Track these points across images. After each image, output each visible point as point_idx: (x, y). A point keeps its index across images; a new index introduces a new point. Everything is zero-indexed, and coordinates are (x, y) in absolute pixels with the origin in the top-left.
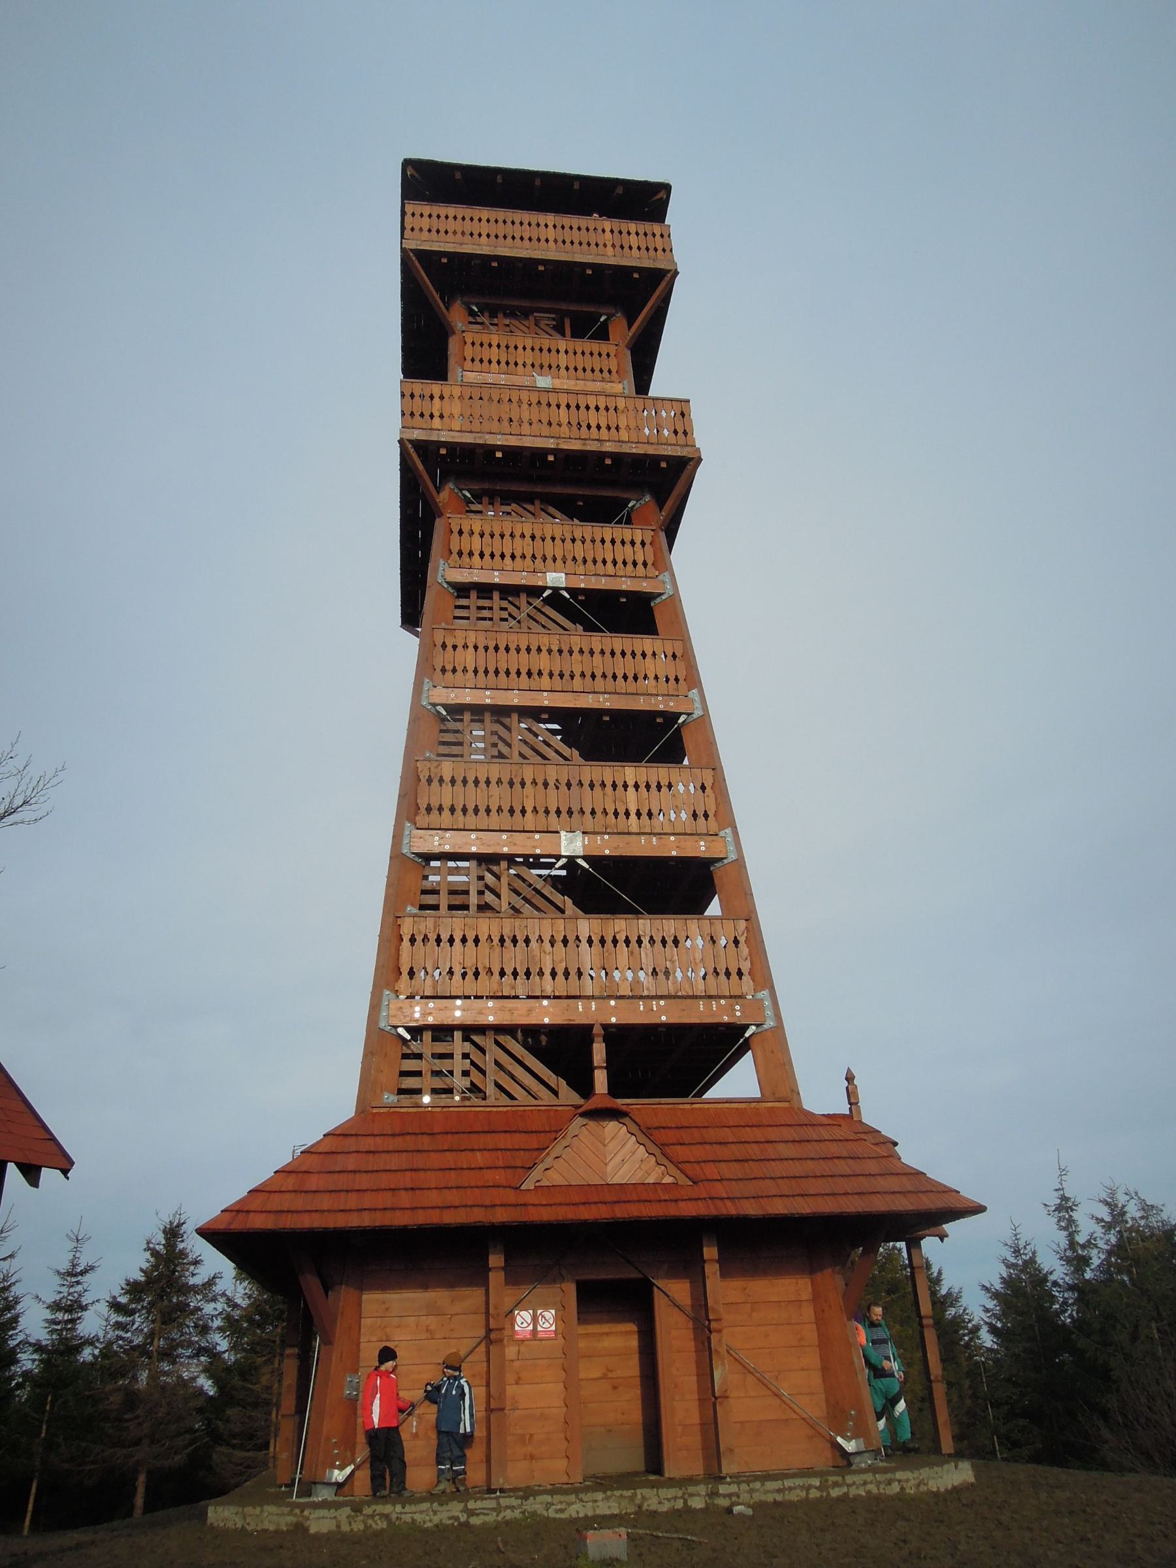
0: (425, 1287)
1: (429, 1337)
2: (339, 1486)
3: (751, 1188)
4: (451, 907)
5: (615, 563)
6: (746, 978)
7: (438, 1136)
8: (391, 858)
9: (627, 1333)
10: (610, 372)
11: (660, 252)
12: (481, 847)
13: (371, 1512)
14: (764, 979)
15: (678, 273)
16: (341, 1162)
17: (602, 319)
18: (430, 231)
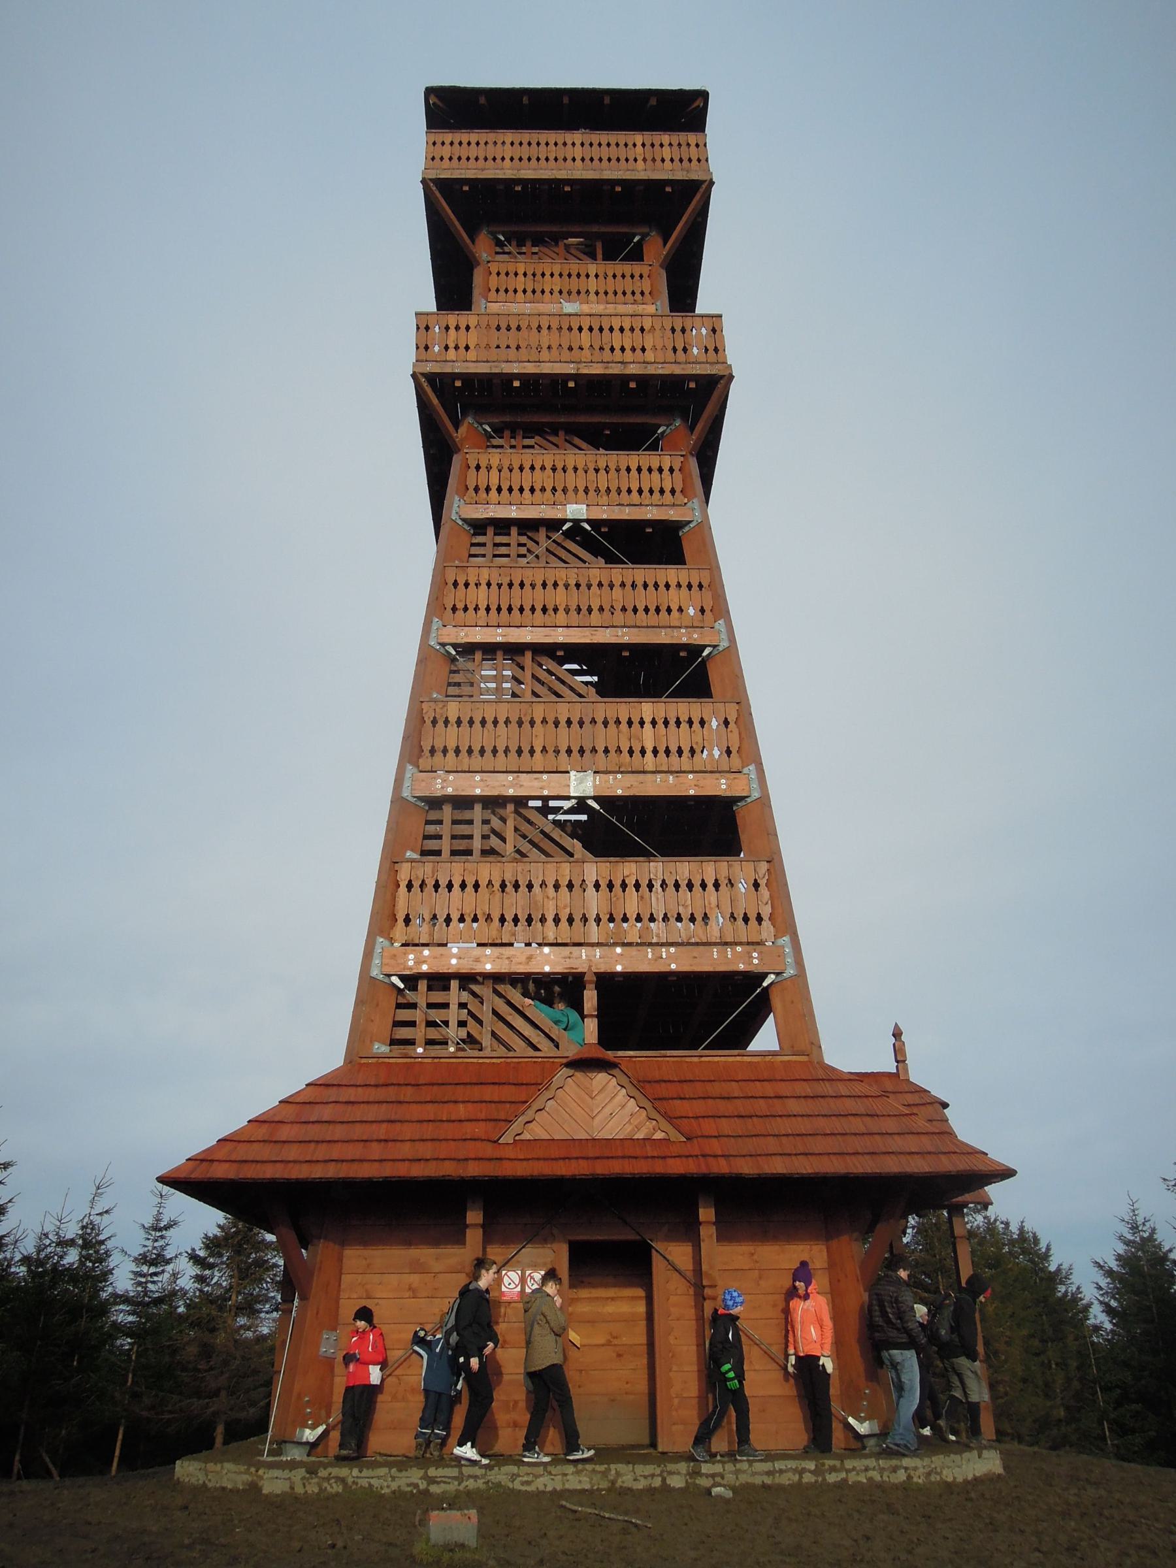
0: (408, 1243)
1: (411, 1295)
2: (313, 1446)
3: (750, 1145)
4: (454, 853)
5: (640, 491)
6: (766, 923)
7: (423, 1087)
8: (391, 802)
9: (633, 1298)
10: (642, 293)
11: (695, 162)
12: (485, 789)
13: (326, 1475)
14: (785, 923)
15: (714, 183)
16: (316, 1113)
17: (636, 239)
18: (451, 159)
